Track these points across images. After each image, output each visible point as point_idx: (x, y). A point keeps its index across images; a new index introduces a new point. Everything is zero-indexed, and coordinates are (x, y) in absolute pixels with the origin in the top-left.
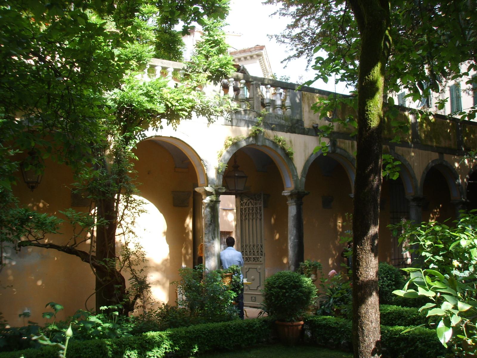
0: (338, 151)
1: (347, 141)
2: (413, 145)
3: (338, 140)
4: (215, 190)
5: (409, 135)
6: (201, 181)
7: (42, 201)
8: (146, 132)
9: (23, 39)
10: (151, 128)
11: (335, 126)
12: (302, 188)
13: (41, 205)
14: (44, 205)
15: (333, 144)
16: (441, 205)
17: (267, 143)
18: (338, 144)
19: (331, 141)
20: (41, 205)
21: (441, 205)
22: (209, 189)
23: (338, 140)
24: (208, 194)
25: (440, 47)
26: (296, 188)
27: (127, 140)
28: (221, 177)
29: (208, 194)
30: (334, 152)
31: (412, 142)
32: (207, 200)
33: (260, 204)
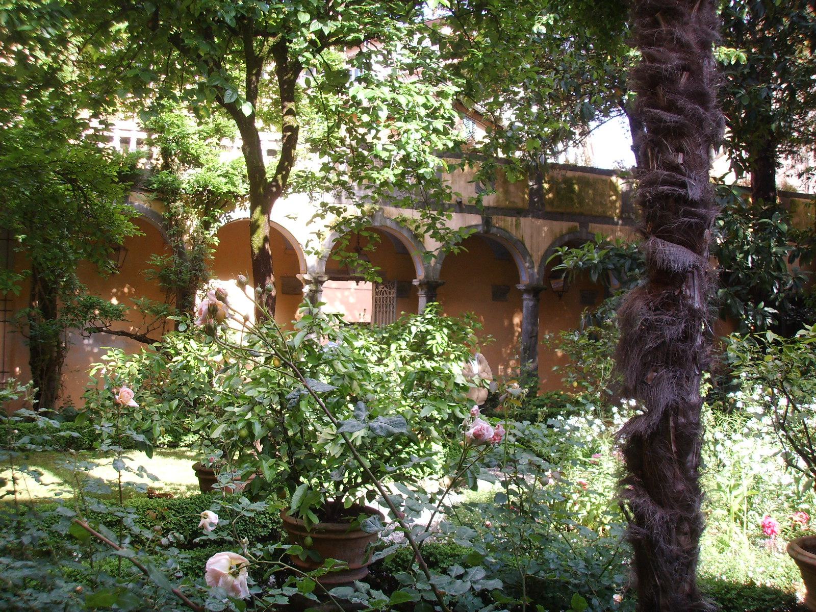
0: (494, 230)
1: (509, 219)
2: (620, 222)
3: (494, 218)
4: (314, 279)
5: (616, 208)
6: (302, 268)
7: (128, 285)
8: (232, 214)
9: (420, 63)
10: (237, 209)
11: (488, 200)
12: (435, 277)
13: (126, 290)
14: (130, 290)
15: (487, 222)
16: (18, 369)
17: (388, 223)
18: (494, 221)
19: (483, 218)
20: (126, 290)
21: (18, 369)
22: (307, 277)
23: (494, 218)
24: (308, 282)
25: (492, 100)
26: (426, 277)
27: (206, 226)
28: (324, 263)
29: (308, 282)
30: (487, 232)
31: (620, 218)
32: (306, 289)
33: (393, 294)
